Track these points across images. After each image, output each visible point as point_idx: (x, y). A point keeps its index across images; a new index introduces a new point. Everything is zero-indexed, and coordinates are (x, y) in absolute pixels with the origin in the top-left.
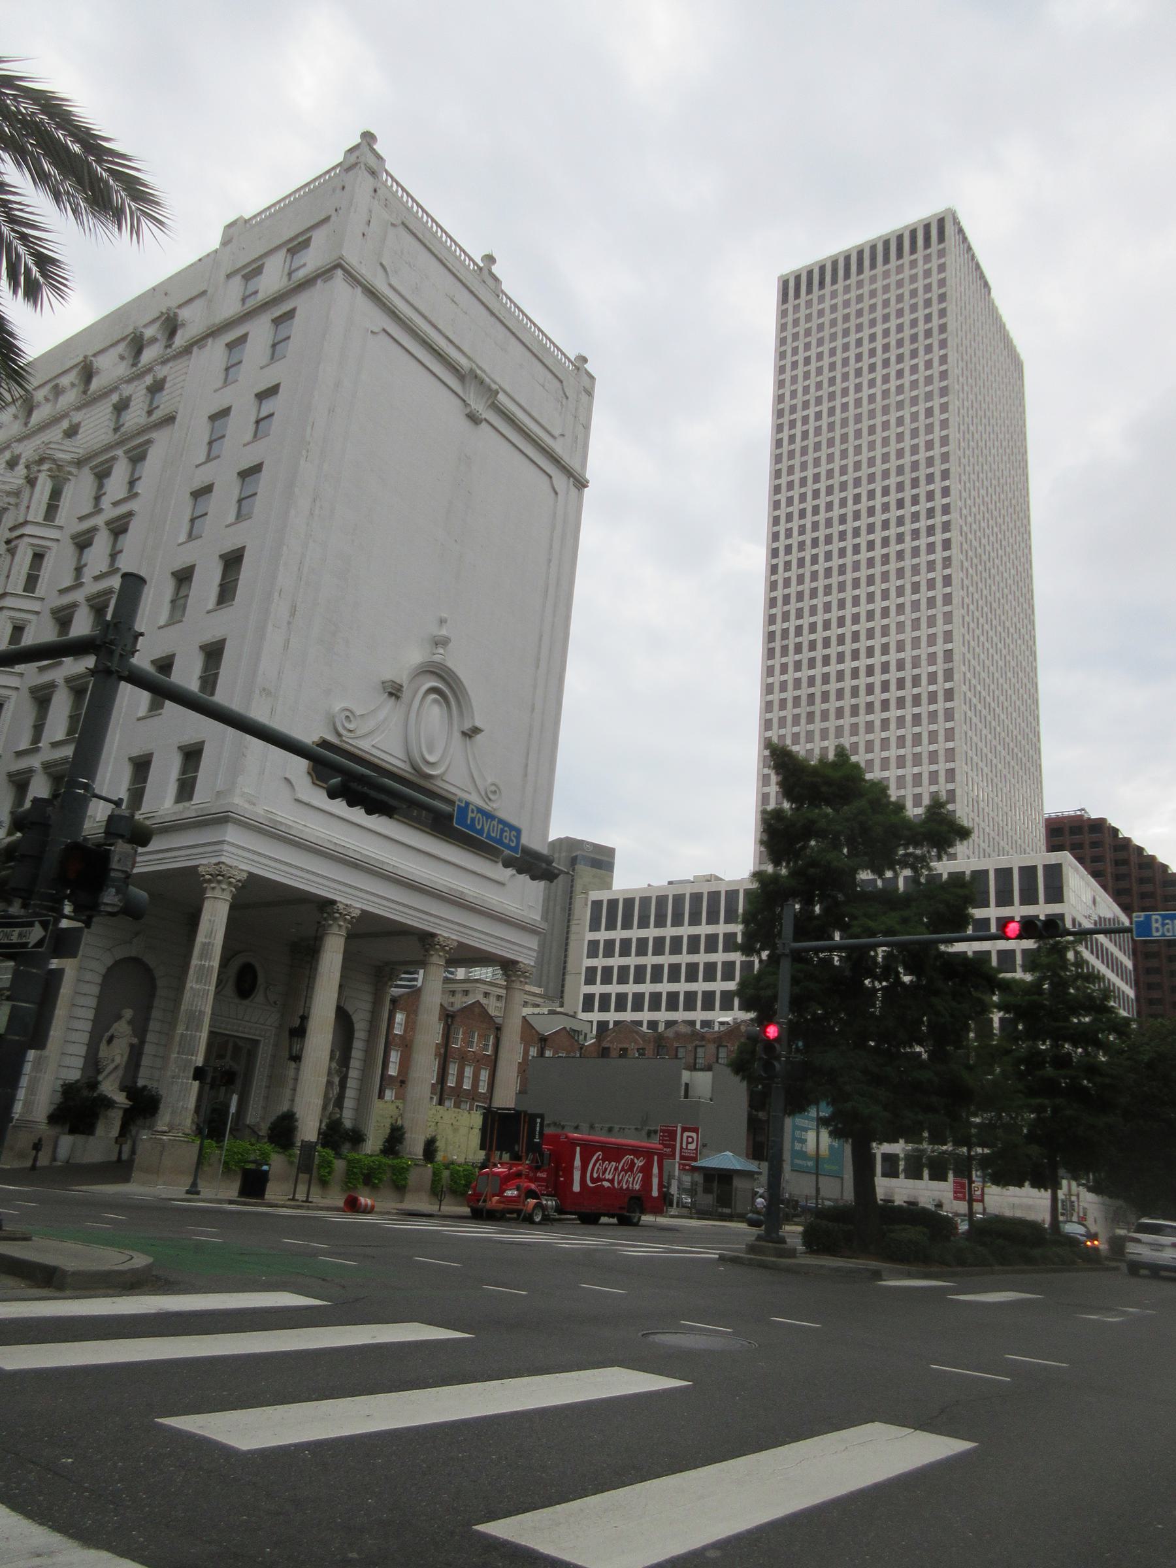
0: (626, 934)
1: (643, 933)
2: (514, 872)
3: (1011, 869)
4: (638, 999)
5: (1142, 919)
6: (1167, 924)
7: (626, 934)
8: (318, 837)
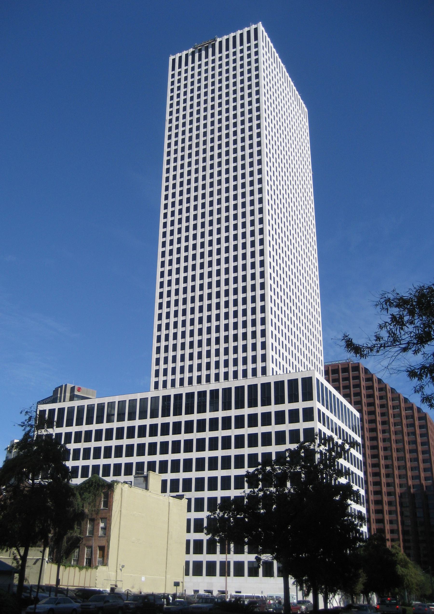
3: (284, 381)
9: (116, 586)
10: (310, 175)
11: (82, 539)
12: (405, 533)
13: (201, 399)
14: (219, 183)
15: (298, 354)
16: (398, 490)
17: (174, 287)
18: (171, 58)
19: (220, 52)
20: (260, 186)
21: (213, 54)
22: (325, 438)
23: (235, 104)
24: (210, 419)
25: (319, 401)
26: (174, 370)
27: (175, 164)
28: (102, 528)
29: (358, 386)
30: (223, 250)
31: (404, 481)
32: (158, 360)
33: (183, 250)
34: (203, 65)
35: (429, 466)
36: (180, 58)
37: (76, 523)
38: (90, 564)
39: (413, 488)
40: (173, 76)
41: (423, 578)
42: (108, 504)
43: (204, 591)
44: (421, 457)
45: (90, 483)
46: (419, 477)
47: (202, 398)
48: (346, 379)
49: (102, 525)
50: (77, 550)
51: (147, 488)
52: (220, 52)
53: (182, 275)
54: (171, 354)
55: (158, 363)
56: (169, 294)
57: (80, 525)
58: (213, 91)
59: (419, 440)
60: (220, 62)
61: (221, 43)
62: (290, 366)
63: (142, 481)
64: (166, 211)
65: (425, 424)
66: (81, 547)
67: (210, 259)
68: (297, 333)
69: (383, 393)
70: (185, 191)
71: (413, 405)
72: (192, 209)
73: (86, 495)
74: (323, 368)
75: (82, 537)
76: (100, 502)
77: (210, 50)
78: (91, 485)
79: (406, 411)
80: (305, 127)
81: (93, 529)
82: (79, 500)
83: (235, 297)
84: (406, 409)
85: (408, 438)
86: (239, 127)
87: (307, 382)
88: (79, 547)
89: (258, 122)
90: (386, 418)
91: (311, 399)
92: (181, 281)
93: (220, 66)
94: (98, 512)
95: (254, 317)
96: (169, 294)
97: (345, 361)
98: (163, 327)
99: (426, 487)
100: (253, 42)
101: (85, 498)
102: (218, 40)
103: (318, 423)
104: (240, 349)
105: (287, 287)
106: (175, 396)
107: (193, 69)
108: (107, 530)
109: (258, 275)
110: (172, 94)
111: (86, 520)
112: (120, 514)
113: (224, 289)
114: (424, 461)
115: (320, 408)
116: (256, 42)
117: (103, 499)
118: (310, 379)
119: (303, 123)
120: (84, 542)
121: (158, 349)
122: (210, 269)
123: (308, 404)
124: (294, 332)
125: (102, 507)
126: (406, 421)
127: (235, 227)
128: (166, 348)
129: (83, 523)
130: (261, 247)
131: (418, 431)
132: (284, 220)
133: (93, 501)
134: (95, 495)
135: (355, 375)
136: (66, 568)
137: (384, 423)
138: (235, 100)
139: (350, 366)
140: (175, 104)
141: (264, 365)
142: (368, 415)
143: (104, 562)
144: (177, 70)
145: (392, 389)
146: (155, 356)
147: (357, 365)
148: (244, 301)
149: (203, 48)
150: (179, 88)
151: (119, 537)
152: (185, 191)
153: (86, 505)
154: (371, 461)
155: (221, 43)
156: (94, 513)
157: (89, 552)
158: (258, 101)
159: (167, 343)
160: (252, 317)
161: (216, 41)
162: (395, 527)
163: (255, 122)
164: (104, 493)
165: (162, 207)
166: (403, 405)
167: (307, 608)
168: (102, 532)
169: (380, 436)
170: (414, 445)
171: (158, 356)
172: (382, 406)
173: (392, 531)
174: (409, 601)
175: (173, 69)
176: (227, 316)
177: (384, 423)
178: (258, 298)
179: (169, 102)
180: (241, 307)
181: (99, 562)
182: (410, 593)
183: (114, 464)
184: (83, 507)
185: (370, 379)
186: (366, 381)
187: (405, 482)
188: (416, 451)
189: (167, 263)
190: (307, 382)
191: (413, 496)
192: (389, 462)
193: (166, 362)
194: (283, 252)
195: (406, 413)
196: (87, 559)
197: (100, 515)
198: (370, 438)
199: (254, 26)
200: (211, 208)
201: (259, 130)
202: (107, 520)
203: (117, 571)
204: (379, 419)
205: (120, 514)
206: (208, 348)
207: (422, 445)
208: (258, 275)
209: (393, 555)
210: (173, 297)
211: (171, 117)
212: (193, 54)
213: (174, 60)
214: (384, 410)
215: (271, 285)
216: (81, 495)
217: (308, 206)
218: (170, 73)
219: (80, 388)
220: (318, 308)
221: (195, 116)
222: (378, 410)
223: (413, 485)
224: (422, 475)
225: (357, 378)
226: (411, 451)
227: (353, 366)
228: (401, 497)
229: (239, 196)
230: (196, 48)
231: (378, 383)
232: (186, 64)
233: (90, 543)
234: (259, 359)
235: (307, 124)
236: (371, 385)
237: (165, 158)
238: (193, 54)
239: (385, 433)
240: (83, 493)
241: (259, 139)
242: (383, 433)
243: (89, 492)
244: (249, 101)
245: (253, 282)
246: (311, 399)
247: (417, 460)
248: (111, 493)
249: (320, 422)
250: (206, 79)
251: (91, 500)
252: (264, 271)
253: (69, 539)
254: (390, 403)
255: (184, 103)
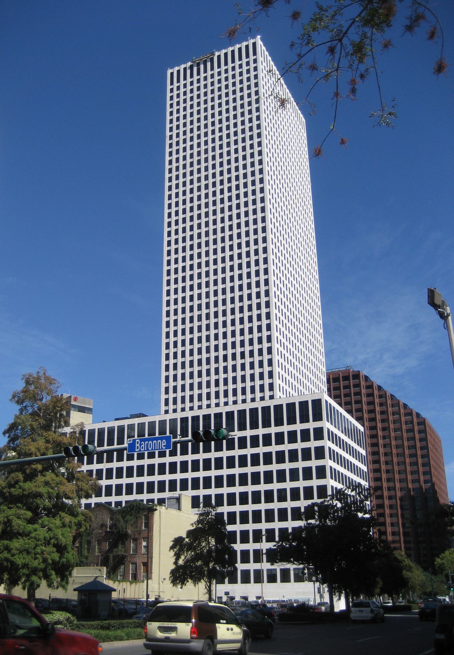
0: (109, 465)
1: (120, 464)
2: (404, 572)
3: (295, 403)
4: (140, 486)
5: (131, 442)
6: (143, 444)
7: (109, 465)
8: (122, 627)
9: (159, 596)
10: (308, 186)
11: (127, 556)
12: (405, 534)
13: (217, 421)
14: (222, 201)
15: (287, 343)
16: (399, 494)
17: (180, 305)
18: (169, 71)
19: (219, 66)
20: (262, 205)
21: (212, 69)
22: (356, 485)
23: (235, 121)
24: (259, 465)
25: (328, 421)
26: (183, 387)
27: (177, 182)
28: (144, 546)
29: (358, 394)
30: (195, 217)
31: (404, 485)
32: (167, 378)
33: (188, 268)
34: (202, 79)
35: (429, 470)
36: (178, 72)
37: (120, 542)
38: (135, 578)
39: (413, 491)
40: (172, 90)
41: (424, 578)
42: (149, 525)
43: (241, 597)
44: (420, 461)
45: (132, 507)
46: (418, 481)
47: (218, 420)
48: (347, 387)
49: (144, 544)
50: (122, 567)
51: (179, 509)
52: (219, 66)
53: (188, 293)
54: (180, 371)
55: (167, 380)
56: (176, 312)
57: (123, 543)
58: (213, 107)
59: (418, 445)
60: (219, 77)
61: (219, 57)
62: (281, 358)
63: (175, 502)
64: (169, 229)
65: (424, 429)
66: (126, 564)
67: (191, 243)
68: (285, 321)
69: (383, 400)
70: (188, 210)
71: (412, 410)
72: (195, 227)
73: (128, 517)
74: (325, 379)
75: (127, 555)
76: (142, 523)
77: (209, 64)
78: (132, 509)
79: (405, 416)
80: (303, 138)
81: (137, 547)
82: (122, 522)
83: (241, 315)
84: (406, 415)
85: (408, 443)
86: (240, 145)
87: (317, 403)
88: (124, 564)
89: (259, 140)
90: (386, 425)
91: (320, 419)
92: (188, 299)
93: (219, 81)
94: (140, 532)
95: (260, 335)
96: (176, 312)
97: (345, 369)
98: (171, 345)
99: (425, 489)
100: (252, 58)
101: (127, 520)
102: (217, 54)
103: (328, 441)
104: (247, 367)
105: (277, 279)
106: (193, 418)
107: (192, 83)
108: (149, 548)
109: (263, 294)
110: (171, 110)
111: (129, 539)
112: (160, 534)
113: (230, 307)
114: (424, 465)
115: (329, 428)
116: (255, 57)
117: (144, 521)
118: (319, 401)
119: (301, 134)
120: (129, 559)
121: (167, 367)
122: (216, 288)
123: (318, 424)
124: (286, 324)
125: (143, 528)
126: (406, 427)
127: (214, 203)
128: (175, 365)
129: (127, 543)
130: (266, 266)
131: (417, 436)
132: (286, 236)
133: (135, 523)
134: (137, 518)
135: (355, 383)
136: (119, 583)
137: (384, 429)
138: (235, 117)
139: (351, 374)
140: (175, 120)
141: (272, 382)
142: (369, 421)
143: (148, 576)
144: (176, 85)
145: (392, 395)
146: (164, 374)
147: (357, 373)
148: (250, 319)
149: (202, 62)
150: (178, 104)
151: (160, 554)
152: (188, 210)
153: (129, 526)
154: (373, 466)
155: (219, 57)
156: (136, 533)
157: (134, 568)
158: (258, 118)
159: (175, 361)
160: (258, 335)
161: (214, 55)
162: (396, 529)
163: (256, 140)
164: (144, 515)
165: (166, 225)
166: (402, 411)
167: (326, 609)
168: (145, 550)
169: (381, 442)
170: (414, 450)
171: (167, 374)
172: (382, 413)
173: (393, 534)
174: (413, 599)
175: (172, 83)
176: (233, 334)
177: (384, 429)
178: (264, 317)
179: (168, 118)
180: (247, 325)
181: (143, 576)
182: (413, 592)
183: (137, 483)
184: (126, 528)
185: (370, 387)
186: (366, 389)
187: (406, 486)
188: (415, 455)
189: (172, 282)
190: (317, 403)
191: (413, 499)
192: (389, 467)
193: (175, 379)
194: (276, 248)
195: (405, 419)
196: (132, 574)
197: (142, 536)
198: (371, 444)
199: (252, 41)
200: (199, 203)
201: (260, 148)
202: (149, 539)
203: (159, 584)
204: (379, 425)
205: (160, 534)
206: (199, 346)
207: (421, 450)
208: (263, 294)
209: (401, 562)
210: (180, 316)
211: (171, 133)
212: (191, 67)
213: (172, 74)
214: (384, 416)
215: (275, 303)
216: (123, 517)
217: (308, 219)
218: (169, 87)
219: (76, 398)
220: (319, 320)
221: (196, 133)
222: (378, 417)
223: (413, 489)
224: (422, 478)
225: (357, 385)
226: (411, 456)
227: (353, 374)
228: (401, 499)
229: (243, 215)
230: (194, 62)
231: (378, 390)
232: (185, 79)
233: (134, 560)
234: (266, 375)
235: (305, 135)
236: (372, 392)
237: (167, 175)
238: (191, 67)
239: (386, 439)
240: (125, 516)
241: (260, 158)
242: (383, 439)
243: (131, 515)
244: (249, 118)
245: (258, 301)
246: (320, 419)
247: (416, 464)
248: (151, 516)
249: (330, 441)
250: (206, 94)
251: (133, 522)
252: (268, 290)
253: (115, 558)
254: (390, 410)
255: (184, 119)
